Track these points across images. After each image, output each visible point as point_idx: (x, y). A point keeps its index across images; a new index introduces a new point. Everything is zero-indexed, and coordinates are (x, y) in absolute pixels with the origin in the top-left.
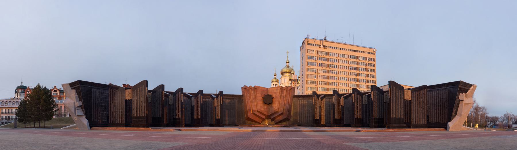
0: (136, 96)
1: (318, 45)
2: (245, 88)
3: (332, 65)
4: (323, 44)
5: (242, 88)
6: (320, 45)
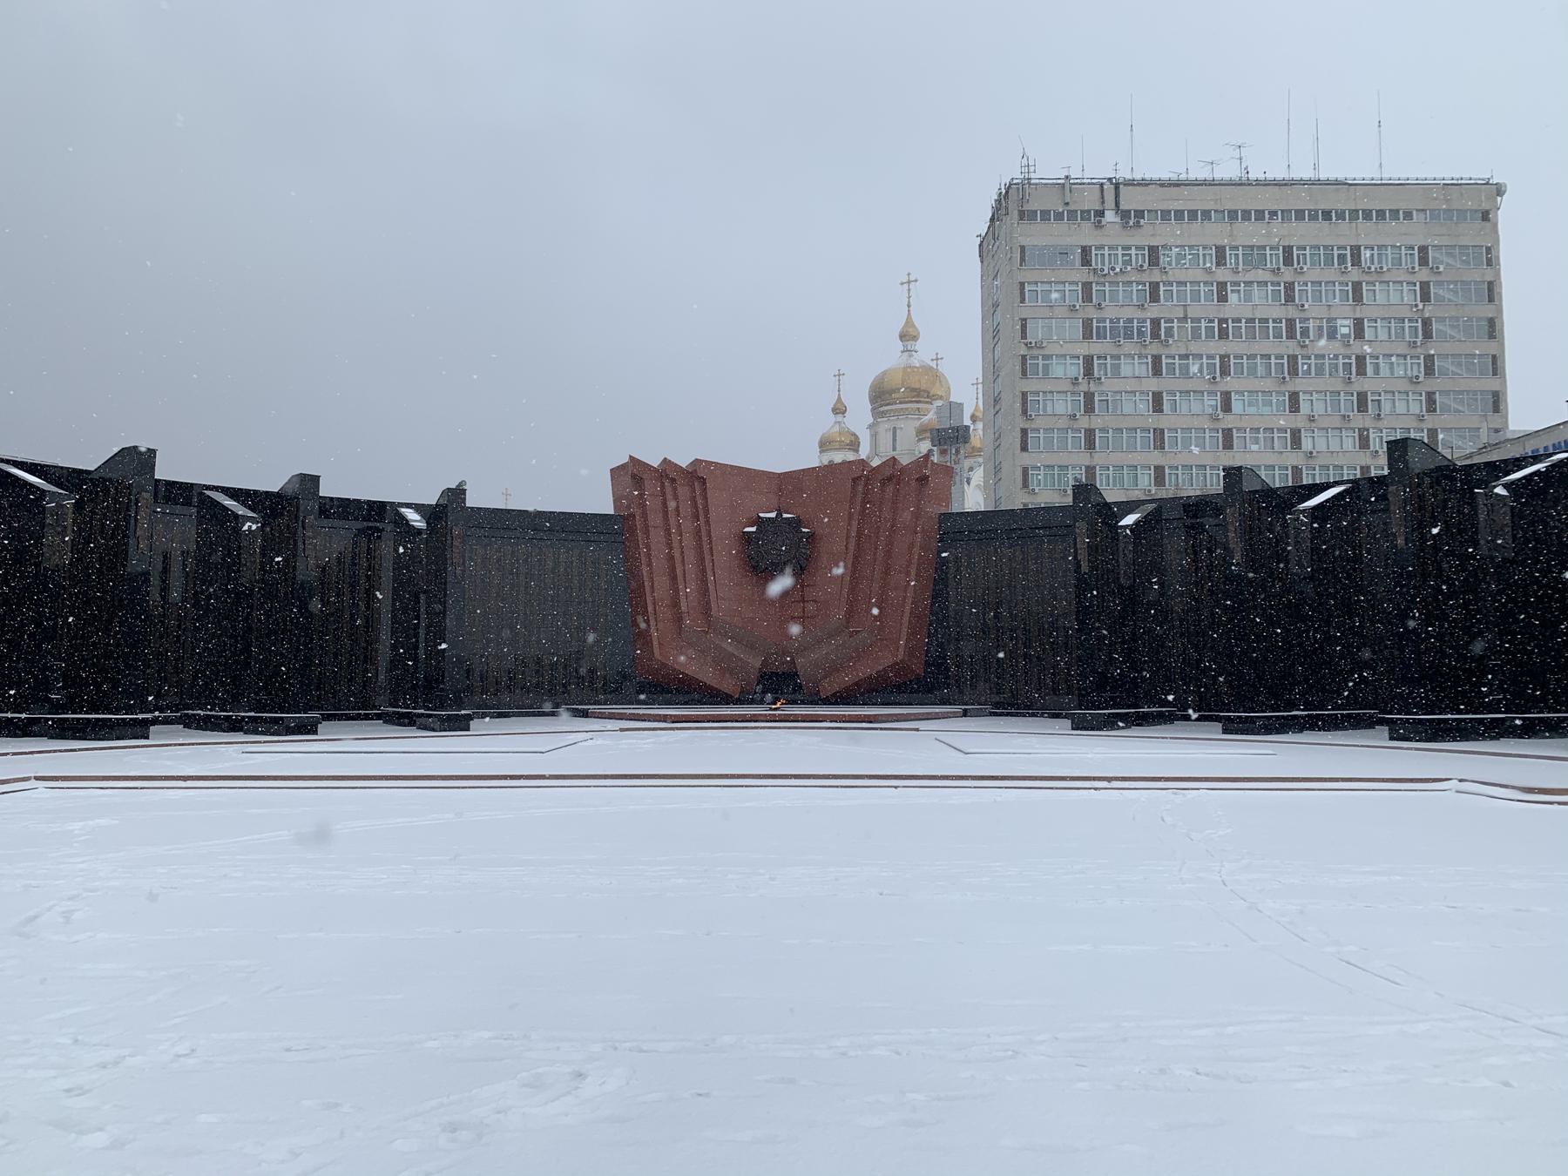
1: (1236, 212)
2: (632, 475)
3: (1179, 320)
4: (1117, 204)
5: (616, 473)
6: (1100, 213)
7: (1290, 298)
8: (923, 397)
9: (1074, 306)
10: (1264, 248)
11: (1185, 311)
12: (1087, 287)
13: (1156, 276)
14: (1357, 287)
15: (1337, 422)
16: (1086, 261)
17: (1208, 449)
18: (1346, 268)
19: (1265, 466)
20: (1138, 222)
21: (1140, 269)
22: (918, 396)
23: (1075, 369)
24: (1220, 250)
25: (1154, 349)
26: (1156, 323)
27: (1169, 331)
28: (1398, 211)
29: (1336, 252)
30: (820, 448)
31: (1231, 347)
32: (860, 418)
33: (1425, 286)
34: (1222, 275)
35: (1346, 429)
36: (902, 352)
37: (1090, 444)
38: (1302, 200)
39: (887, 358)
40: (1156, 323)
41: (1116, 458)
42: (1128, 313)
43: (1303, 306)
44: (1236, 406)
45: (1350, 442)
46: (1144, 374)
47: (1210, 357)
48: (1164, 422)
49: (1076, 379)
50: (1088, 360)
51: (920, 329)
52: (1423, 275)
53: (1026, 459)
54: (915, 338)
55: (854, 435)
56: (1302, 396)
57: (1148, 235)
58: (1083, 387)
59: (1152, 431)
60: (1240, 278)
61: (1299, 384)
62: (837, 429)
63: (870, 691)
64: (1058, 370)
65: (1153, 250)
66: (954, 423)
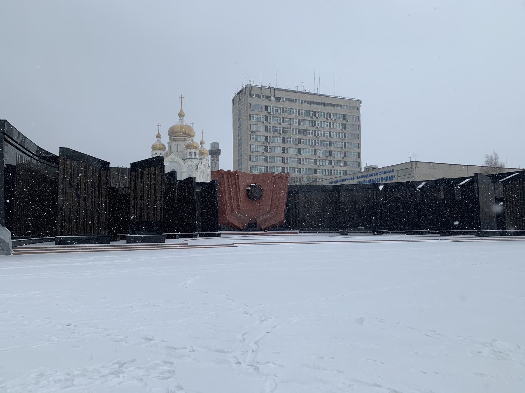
0: (141, 182)
4: (274, 96)
6: (270, 97)
7: (315, 125)
8: (186, 135)
9: (264, 122)
10: (309, 111)
11: (291, 126)
12: (267, 117)
13: (283, 116)
14: (330, 123)
15: (325, 158)
16: (266, 110)
17: (295, 163)
18: (328, 118)
19: (308, 168)
20: (280, 101)
21: (280, 114)
22: (185, 135)
23: (263, 139)
24: (299, 111)
25: (283, 136)
26: (283, 128)
27: (286, 131)
28: (339, 105)
29: (325, 114)
30: (152, 149)
31: (301, 137)
32: (165, 140)
33: (345, 125)
34: (299, 117)
35: (327, 160)
36: (179, 120)
37: (267, 161)
38: (317, 99)
39: (175, 121)
40: (283, 128)
41: (273, 164)
42: (277, 125)
43: (318, 127)
44: (302, 152)
45: (327, 163)
46: (280, 142)
47: (296, 139)
48: (285, 155)
49: (264, 142)
50: (267, 137)
51: (185, 113)
52: (344, 122)
53: (251, 163)
54: (184, 116)
55: (164, 145)
56: (317, 151)
57: (283, 104)
58: (265, 145)
59: (282, 158)
60: (304, 118)
61: (317, 148)
62: (158, 143)
63: (272, 227)
64: (259, 139)
65: (283, 109)
66: (216, 149)
